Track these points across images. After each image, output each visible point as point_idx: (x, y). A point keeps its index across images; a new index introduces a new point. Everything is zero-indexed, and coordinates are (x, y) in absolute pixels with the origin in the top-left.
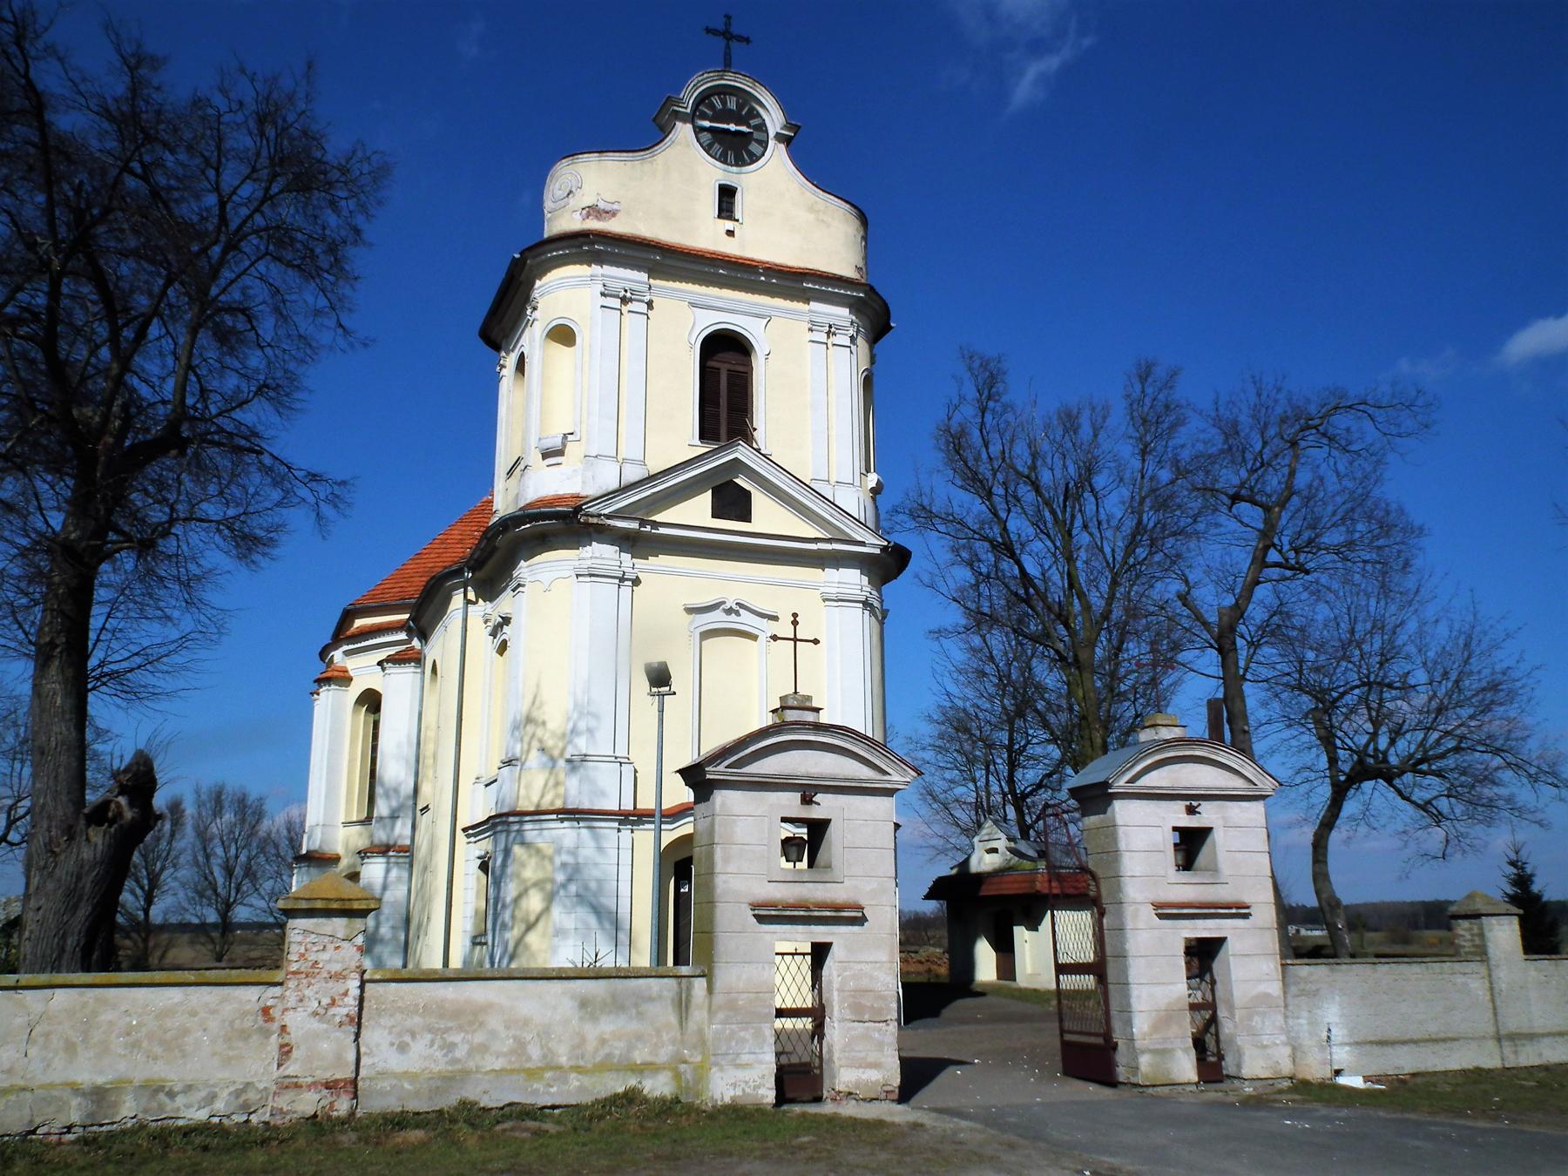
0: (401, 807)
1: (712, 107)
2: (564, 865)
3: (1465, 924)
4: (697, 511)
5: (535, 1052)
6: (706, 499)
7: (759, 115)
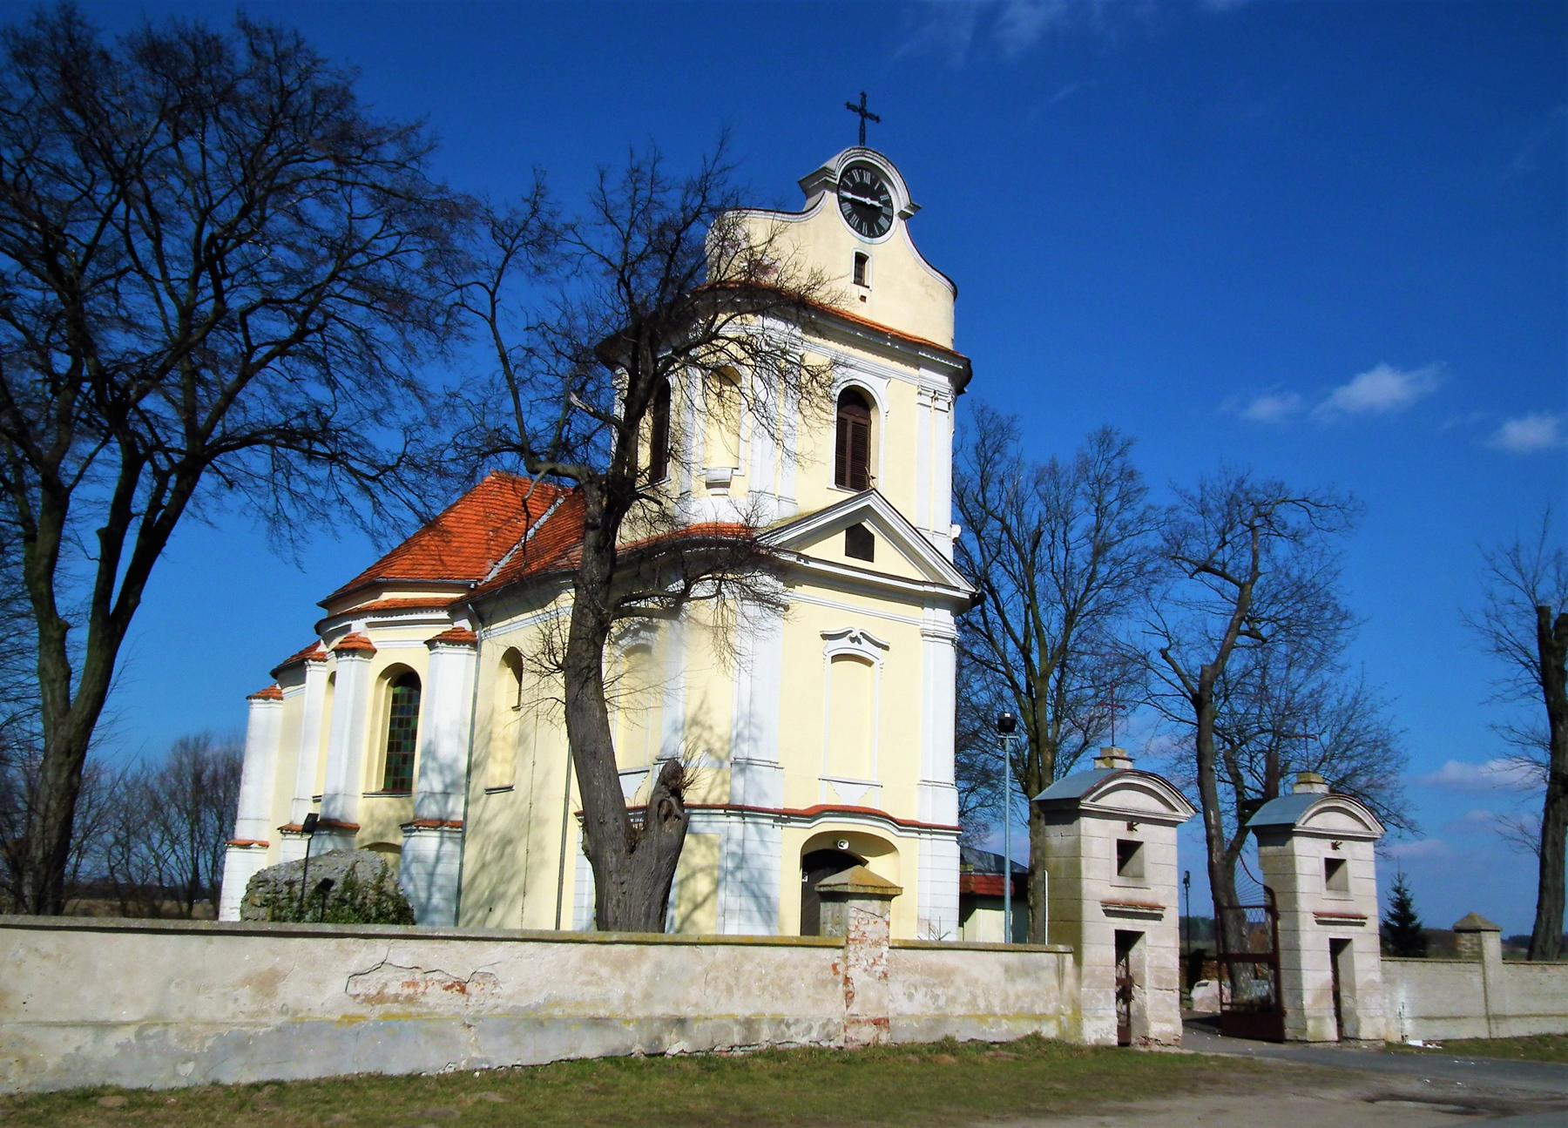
0: (454, 784)
1: (852, 179)
2: (733, 854)
3: (1467, 936)
4: (832, 549)
5: (982, 1003)
6: (840, 539)
7: (886, 192)
